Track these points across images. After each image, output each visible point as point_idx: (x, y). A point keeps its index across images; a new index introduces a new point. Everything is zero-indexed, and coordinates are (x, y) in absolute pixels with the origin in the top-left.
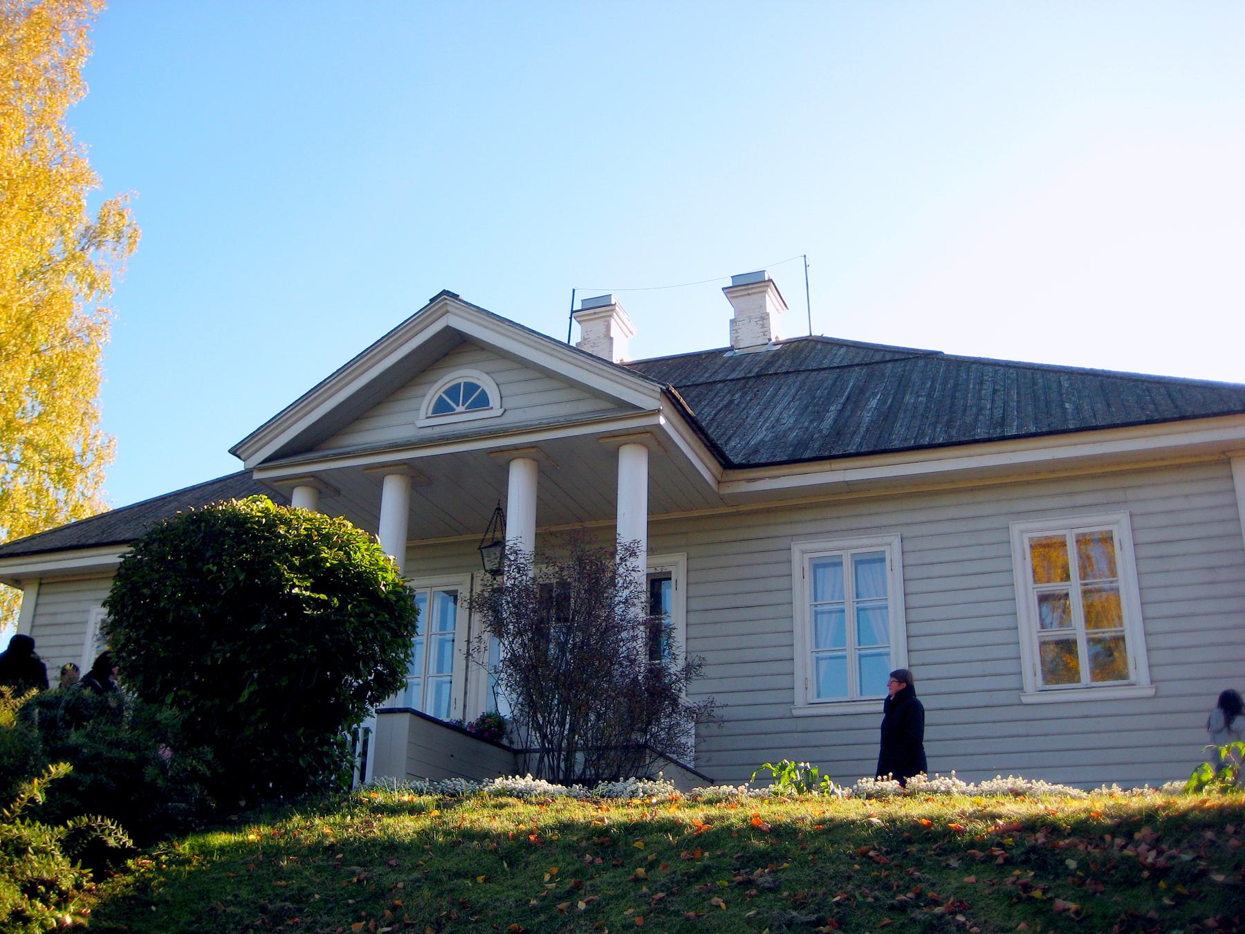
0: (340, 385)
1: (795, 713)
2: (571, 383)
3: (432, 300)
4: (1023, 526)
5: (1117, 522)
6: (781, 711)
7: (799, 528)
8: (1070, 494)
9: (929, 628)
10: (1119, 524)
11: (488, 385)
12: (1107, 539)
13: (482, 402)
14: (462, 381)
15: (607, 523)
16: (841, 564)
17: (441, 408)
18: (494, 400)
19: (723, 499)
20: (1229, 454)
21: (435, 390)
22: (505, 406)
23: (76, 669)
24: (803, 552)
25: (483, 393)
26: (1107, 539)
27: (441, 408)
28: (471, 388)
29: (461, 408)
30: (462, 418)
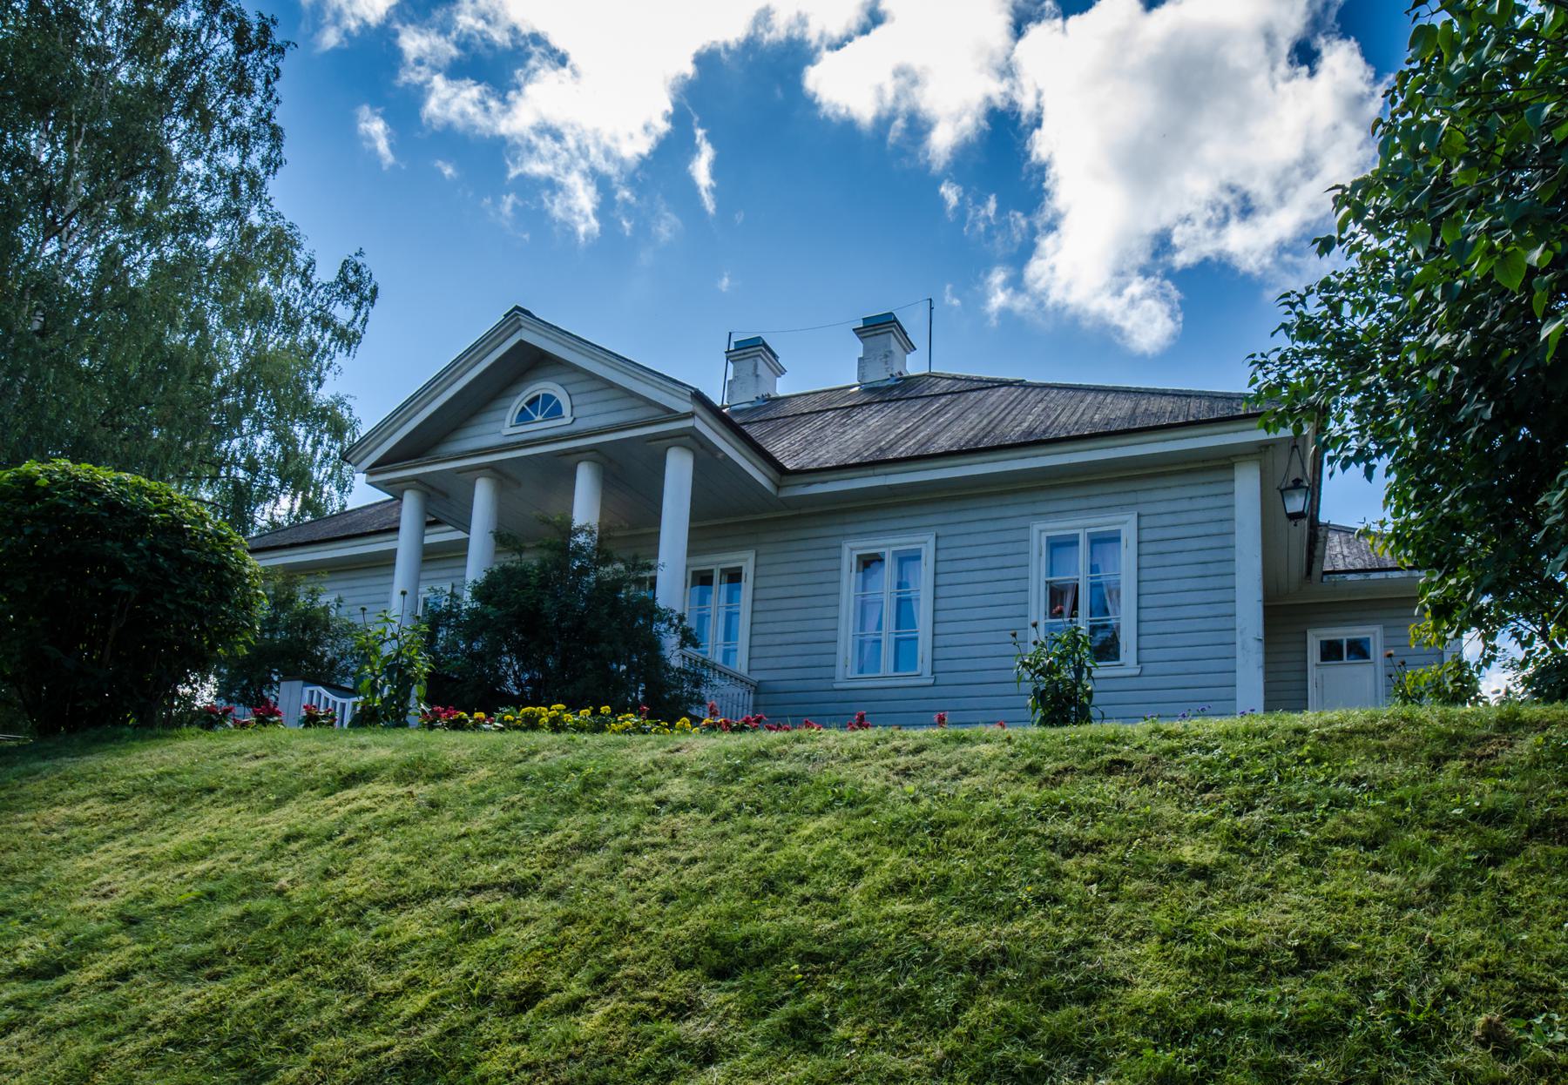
0: (439, 389)
1: (836, 686)
2: (631, 394)
3: (506, 316)
4: (1042, 526)
5: (1125, 522)
6: (824, 684)
7: (850, 529)
8: (1087, 497)
9: (769, 616)
10: (1126, 524)
11: (561, 396)
12: (1114, 538)
13: (556, 412)
14: (540, 393)
15: (653, 530)
16: (1077, 543)
17: (524, 417)
18: (566, 410)
19: (783, 500)
20: (1234, 460)
21: (518, 402)
22: (575, 415)
23: (918, 127)
24: (852, 549)
25: (558, 403)
26: (1114, 538)
27: (524, 417)
28: (548, 398)
29: (539, 418)
30: (540, 426)
